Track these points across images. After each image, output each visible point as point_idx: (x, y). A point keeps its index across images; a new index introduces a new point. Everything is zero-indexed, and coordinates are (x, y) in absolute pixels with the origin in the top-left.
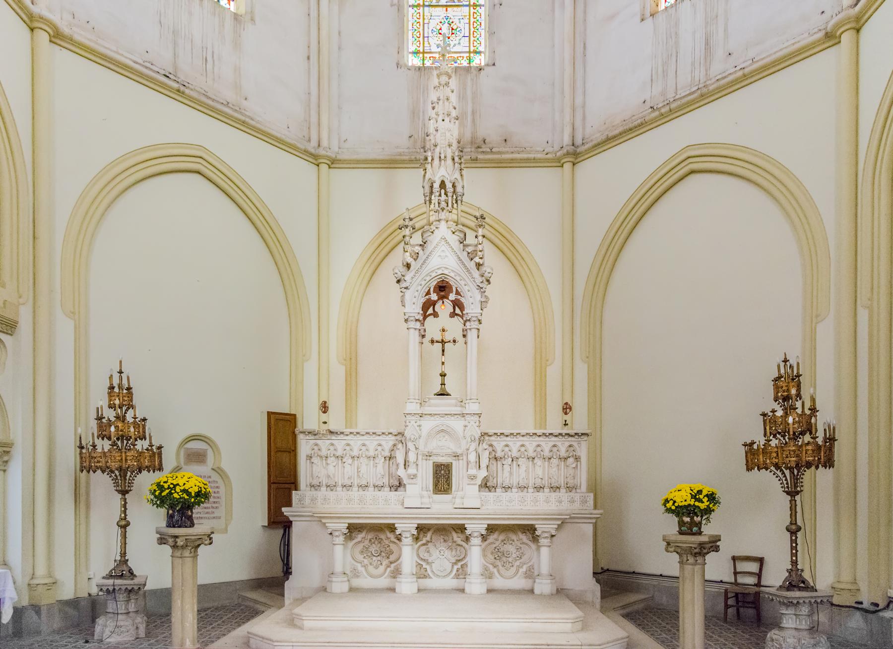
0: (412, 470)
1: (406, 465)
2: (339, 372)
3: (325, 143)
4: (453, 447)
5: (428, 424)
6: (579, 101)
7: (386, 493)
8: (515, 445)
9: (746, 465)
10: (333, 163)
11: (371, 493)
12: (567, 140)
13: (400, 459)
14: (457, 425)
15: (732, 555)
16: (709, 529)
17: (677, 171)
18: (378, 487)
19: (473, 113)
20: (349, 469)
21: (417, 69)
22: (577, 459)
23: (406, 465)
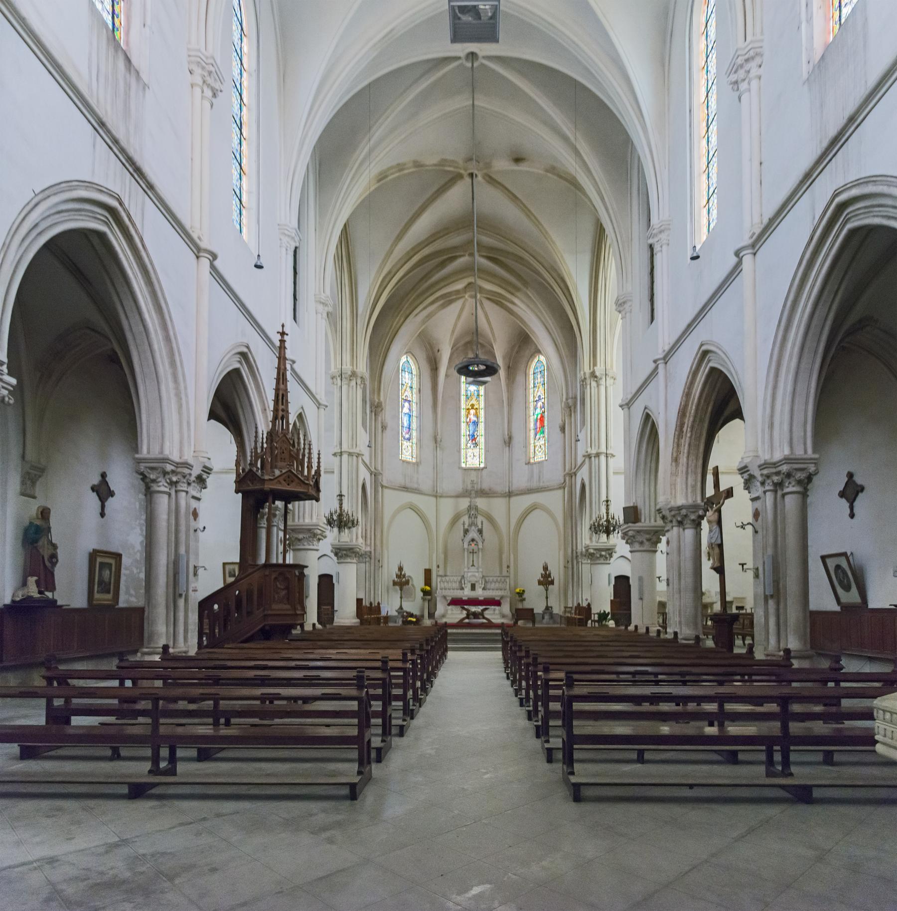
0: (466, 585)
1: (465, 584)
2: (442, 556)
3: (438, 491)
4: (476, 579)
5: (469, 574)
6: (511, 480)
7: (459, 591)
8: (491, 579)
9: (702, 529)
10: (441, 497)
11: (456, 591)
12: (507, 491)
13: (463, 582)
14: (477, 574)
15: (114, 497)
16: (524, 597)
17: (615, 232)
18: (457, 589)
19: (481, 482)
20: (450, 585)
21: (527, 649)
22: (506, 582)
23: (465, 584)
